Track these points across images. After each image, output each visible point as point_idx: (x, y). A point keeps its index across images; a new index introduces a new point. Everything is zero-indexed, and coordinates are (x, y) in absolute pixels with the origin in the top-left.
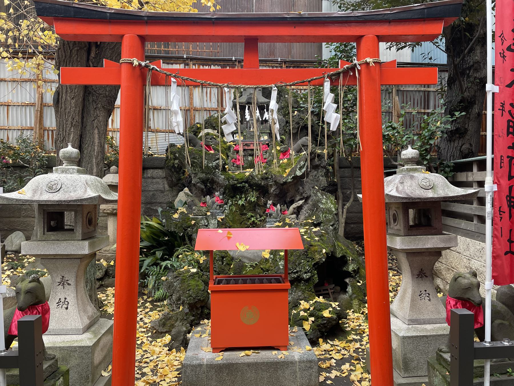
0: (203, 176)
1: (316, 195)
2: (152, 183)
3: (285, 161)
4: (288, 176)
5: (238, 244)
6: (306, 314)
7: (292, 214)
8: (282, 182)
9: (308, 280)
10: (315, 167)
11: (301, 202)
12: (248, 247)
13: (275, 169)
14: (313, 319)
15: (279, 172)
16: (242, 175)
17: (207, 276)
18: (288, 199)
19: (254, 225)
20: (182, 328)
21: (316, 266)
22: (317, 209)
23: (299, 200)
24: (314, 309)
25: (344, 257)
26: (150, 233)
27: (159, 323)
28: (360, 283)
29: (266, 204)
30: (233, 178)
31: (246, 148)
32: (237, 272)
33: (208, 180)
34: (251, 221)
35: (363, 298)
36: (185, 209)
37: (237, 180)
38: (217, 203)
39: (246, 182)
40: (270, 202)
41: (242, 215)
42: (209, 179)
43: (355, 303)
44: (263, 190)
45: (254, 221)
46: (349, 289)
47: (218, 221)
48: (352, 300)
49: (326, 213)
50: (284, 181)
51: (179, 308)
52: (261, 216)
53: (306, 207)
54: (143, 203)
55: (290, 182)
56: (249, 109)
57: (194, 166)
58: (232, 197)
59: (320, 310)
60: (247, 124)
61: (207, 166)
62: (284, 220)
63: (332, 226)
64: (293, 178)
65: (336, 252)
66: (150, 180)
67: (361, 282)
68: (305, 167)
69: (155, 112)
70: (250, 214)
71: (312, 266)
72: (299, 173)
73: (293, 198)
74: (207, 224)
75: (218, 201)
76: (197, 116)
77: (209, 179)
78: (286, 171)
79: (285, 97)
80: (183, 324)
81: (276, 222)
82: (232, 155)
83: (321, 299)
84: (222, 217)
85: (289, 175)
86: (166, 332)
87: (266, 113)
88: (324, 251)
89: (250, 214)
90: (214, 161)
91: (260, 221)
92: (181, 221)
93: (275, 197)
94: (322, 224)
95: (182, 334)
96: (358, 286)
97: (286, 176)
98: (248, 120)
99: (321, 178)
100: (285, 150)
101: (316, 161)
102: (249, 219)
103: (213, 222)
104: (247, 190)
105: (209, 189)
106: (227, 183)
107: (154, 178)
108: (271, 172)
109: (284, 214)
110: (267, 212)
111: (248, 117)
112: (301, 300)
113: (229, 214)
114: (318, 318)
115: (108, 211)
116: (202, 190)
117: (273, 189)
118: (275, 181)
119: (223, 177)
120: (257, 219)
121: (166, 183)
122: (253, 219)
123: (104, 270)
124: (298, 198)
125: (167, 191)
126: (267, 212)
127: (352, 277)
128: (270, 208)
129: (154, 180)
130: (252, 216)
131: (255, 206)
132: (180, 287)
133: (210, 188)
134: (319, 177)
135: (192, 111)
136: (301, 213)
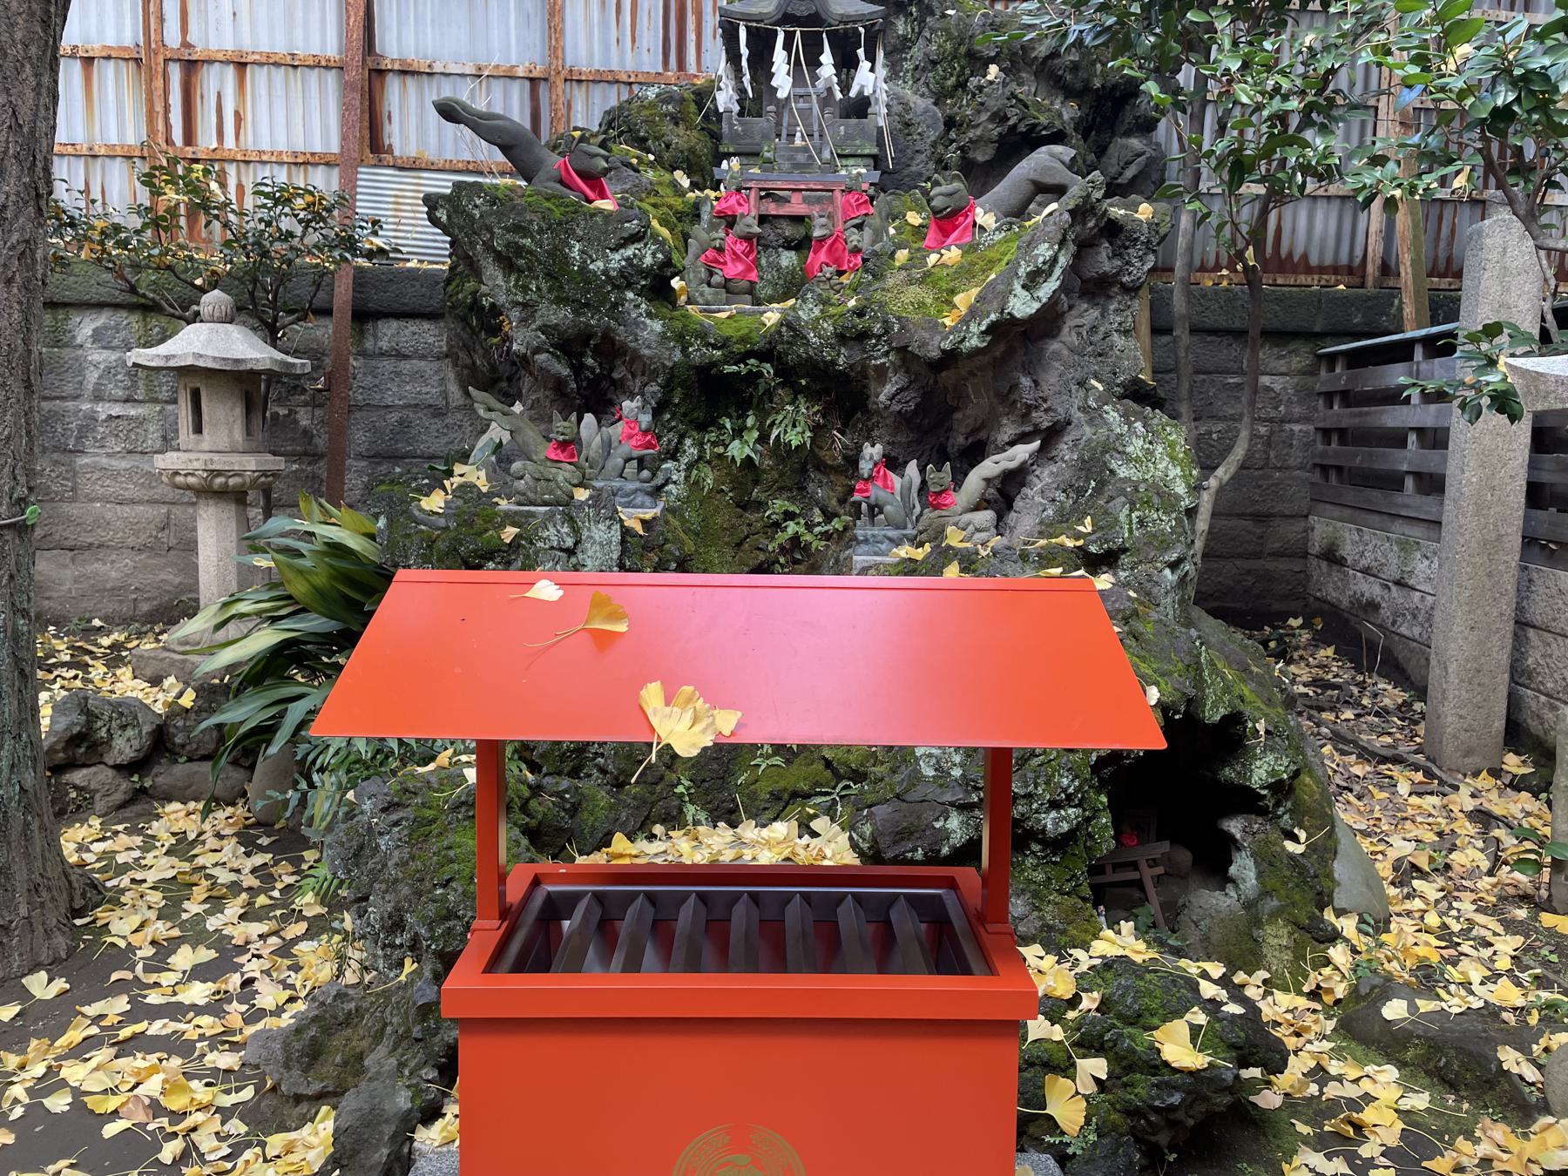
0: (560, 315)
1: (1094, 416)
2: (398, 374)
3: (953, 254)
4: (965, 321)
5: (652, 695)
6: (1057, 1033)
7: (977, 508)
8: (935, 354)
9: (1060, 844)
10: (1089, 286)
11: (1022, 452)
12: (727, 723)
13: (903, 298)
14: (1097, 1066)
15: (922, 305)
16: (745, 324)
17: (559, 794)
18: (959, 440)
19: (799, 558)
20: (394, 1091)
21: (1107, 771)
22: (1102, 484)
23: (1012, 444)
24: (1104, 1007)
25: (1234, 720)
26: (334, 578)
27: (286, 1046)
28: (1295, 839)
29: (853, 461)
30: (702, 335)
31: (772, 208)
32: (707, 775)
33: (585, 336)
34: (782, 538)
35: (1312, 918)
36: (482, 474)
37: (724, 344)
38: (626, 449)
39: (765, 355)
40: (873, 452)
41: (744, 508)
42: (590, 336)
43: (1276, 937)
44: (841, 395)
45: (795, 539)
46: (1244, 868)
47: (626, 532)
48: (1258, 923)
49: (1147, 503)
50: (946, 345)
51: (401, 965)
52: (829, 516)
53: (1045, 476)
54: (360, 456)
55: (977, 352)
56: (788, 46)
57: (520, 271)
58: (702, 427)
59: (1139, 1020)
60: (779, 114)
61: (583, 268)
62: (940, 534)
63: (1173, 566)
64: (993, 329)
65: (1204, 698)
66: (387, 365)
67: (1302, 835)
68: (1058, 272)
69: (410, 80)
70: (779, 505)
71: (1087, 773)
72: (1022, 305)
73: (982, 435)
74: (569, 542)
75: (630, 437)
76: (579, 106)
77: (590, 336)
78: (957, 299)
79: (944, 16)
80: (402, 1065)
81: (897, 543)
82: (704, 236)
83: (1121, 941)
84: (648, 514)
85: (973, 313)
86: (320, 1097)
87: (865, 65)
88: (1153, 695)
89: (779, 505)
90: (615, 250)
91: (826, 536)
92: (453, 525)
93: (897, 430)
94: (1125, 559)
95: (388, 1130)
96: (1291, 857)
97: (958, 321)
98: (782, 94)
99: (1118, 341)
100: (953, 203)
101: (1103, 261)
102: (776, 525)
103: (601, 537)
104: (769, 394)
105: (595, 382)
106: (677, 356)
107: (406, 357)
108: (882, 305)
109: (937, 507)
110: (857, 497)
111: (782, 80)
112: (1027, 941)
113: (687, 500)
114: (1129, 1069)
115: (191, 480)
116: (559, 385)
117: (889, 389)
118: (903, 350)
119: (657, 326)
120: (809, 527)
121: (451, 376)
122: (792, 528)
123: (147, 729)
124: (1008, 430)
125: (458, 408)
126: (857, 497)
127: (1263, 812)
128: (871, 478)
129: (405, 366)
130: (789, 516)
131: (803, 470)
132: (402, 864)
133: (598, 379)
134: (1107, 335)
135: (560, 84)
136: (1018, 504)
